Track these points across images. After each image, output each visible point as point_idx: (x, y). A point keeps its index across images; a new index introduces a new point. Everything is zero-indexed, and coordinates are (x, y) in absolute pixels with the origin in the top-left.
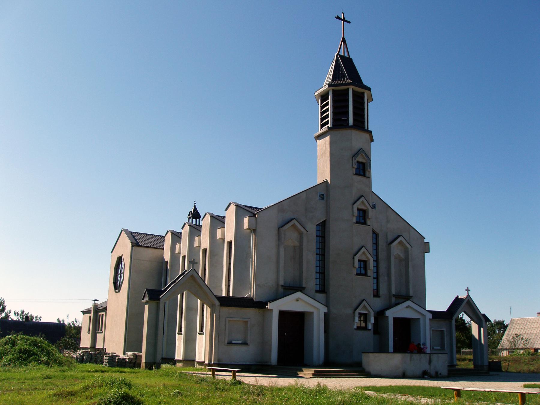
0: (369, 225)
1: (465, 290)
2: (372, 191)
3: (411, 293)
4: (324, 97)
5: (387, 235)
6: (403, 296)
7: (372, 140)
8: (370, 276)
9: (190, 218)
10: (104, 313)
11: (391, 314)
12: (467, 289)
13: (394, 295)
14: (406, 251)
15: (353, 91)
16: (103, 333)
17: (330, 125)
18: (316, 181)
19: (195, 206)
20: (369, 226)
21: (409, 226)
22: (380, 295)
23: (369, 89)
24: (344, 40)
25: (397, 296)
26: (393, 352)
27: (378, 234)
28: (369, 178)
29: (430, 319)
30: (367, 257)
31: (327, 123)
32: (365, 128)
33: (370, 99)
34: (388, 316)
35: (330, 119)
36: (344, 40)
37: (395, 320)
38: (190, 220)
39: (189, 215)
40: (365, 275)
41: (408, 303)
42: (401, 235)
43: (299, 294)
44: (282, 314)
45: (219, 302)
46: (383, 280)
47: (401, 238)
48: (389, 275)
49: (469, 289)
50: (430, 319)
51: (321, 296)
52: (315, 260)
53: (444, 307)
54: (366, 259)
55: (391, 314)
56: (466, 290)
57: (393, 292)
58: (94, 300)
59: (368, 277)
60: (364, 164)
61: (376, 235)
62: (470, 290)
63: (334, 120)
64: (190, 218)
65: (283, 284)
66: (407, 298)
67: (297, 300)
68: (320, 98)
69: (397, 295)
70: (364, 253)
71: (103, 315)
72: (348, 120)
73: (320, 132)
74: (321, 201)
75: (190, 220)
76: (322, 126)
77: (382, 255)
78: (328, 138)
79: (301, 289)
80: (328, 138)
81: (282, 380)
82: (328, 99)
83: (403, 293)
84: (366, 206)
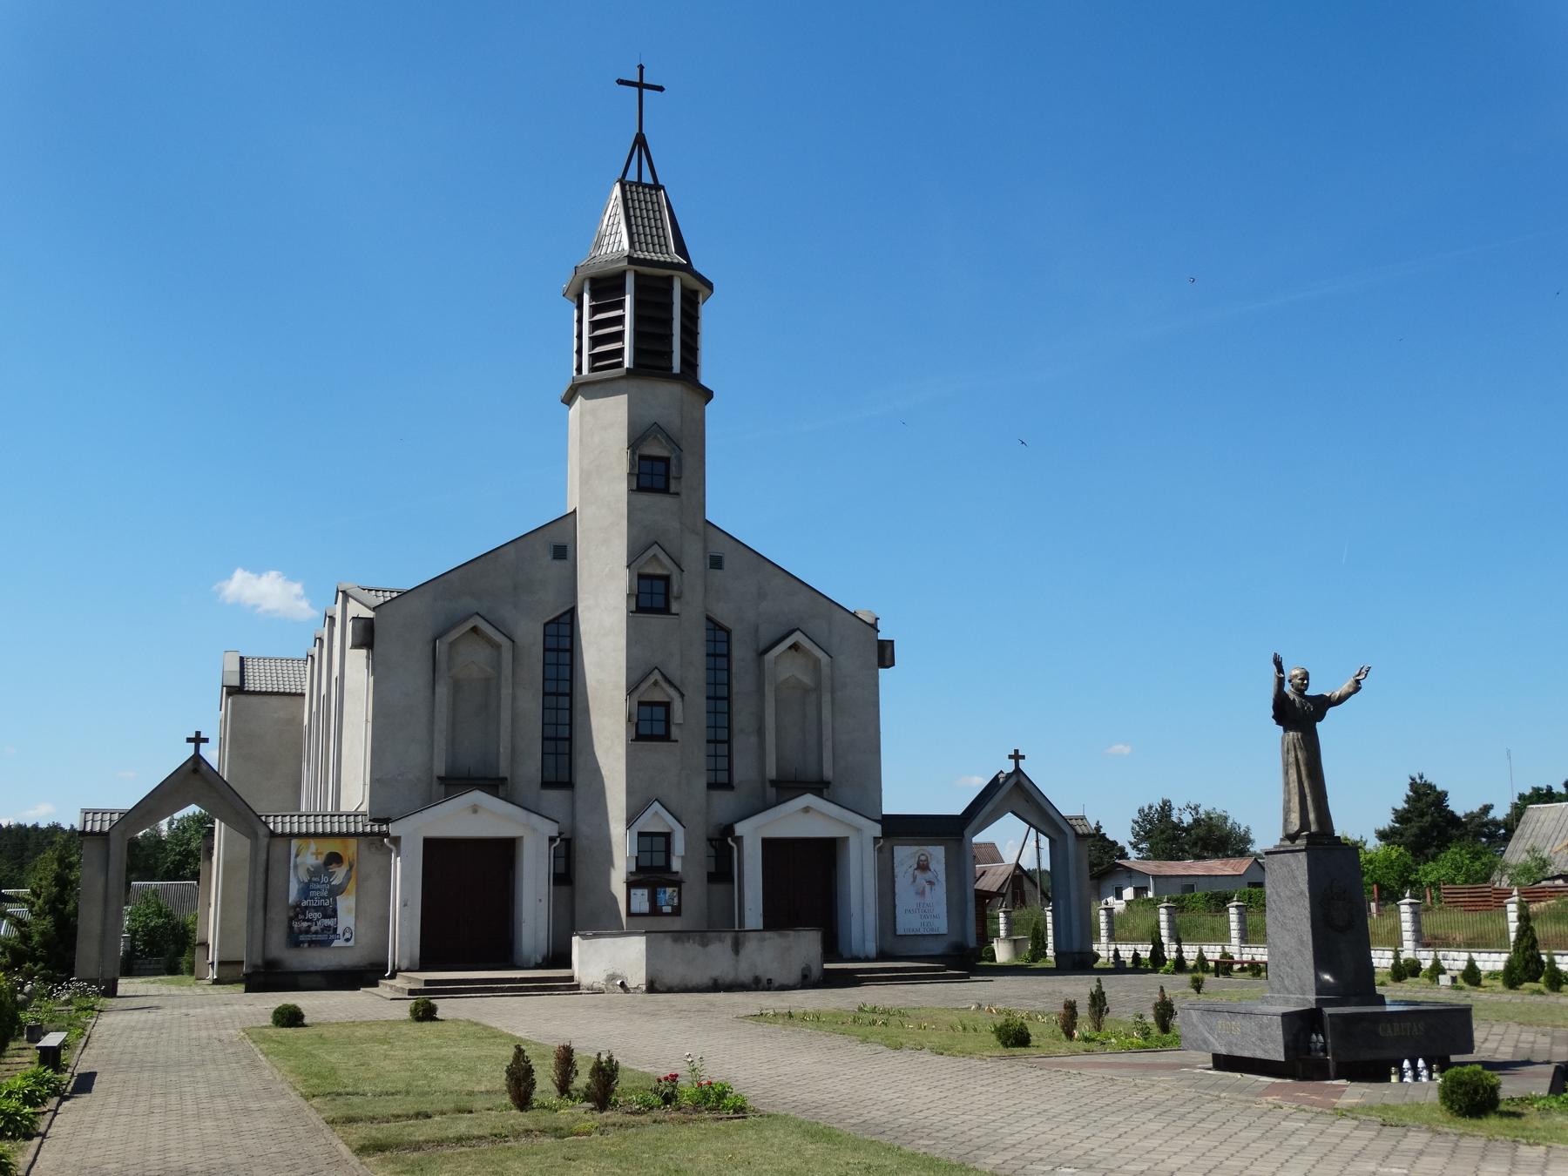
0: (677, 614)
2: (707, 521)
3: (828, 773)
5: (757, 631)
8: (677, 741)
11: (752, 833)
12: (193, 736)
13: (773, 783)
16: (1202, 980)
17: (627, 361)
18: (566, 509)
20: (676, 617)
21: (829, 602)
22: (735, 785)
23: (709, 286)
24: (640, 142)
26: (762, 928)
29: (876, 839)
30: (668, 695)
32: (672, 368)
34: (742, 837)
36: (640, 142)
42: (798, 629)
44: (771, 847)
47: (797, 637)
48: (760, 732)
50: (876, 839)
52: (705, 698)
54: (667, 700)
59: (673, 744)
63: (638, 352)
65: (443, 774)
70: (656, 683)
74: (558, 562)
77: (742, 684)
84: (665, 567)
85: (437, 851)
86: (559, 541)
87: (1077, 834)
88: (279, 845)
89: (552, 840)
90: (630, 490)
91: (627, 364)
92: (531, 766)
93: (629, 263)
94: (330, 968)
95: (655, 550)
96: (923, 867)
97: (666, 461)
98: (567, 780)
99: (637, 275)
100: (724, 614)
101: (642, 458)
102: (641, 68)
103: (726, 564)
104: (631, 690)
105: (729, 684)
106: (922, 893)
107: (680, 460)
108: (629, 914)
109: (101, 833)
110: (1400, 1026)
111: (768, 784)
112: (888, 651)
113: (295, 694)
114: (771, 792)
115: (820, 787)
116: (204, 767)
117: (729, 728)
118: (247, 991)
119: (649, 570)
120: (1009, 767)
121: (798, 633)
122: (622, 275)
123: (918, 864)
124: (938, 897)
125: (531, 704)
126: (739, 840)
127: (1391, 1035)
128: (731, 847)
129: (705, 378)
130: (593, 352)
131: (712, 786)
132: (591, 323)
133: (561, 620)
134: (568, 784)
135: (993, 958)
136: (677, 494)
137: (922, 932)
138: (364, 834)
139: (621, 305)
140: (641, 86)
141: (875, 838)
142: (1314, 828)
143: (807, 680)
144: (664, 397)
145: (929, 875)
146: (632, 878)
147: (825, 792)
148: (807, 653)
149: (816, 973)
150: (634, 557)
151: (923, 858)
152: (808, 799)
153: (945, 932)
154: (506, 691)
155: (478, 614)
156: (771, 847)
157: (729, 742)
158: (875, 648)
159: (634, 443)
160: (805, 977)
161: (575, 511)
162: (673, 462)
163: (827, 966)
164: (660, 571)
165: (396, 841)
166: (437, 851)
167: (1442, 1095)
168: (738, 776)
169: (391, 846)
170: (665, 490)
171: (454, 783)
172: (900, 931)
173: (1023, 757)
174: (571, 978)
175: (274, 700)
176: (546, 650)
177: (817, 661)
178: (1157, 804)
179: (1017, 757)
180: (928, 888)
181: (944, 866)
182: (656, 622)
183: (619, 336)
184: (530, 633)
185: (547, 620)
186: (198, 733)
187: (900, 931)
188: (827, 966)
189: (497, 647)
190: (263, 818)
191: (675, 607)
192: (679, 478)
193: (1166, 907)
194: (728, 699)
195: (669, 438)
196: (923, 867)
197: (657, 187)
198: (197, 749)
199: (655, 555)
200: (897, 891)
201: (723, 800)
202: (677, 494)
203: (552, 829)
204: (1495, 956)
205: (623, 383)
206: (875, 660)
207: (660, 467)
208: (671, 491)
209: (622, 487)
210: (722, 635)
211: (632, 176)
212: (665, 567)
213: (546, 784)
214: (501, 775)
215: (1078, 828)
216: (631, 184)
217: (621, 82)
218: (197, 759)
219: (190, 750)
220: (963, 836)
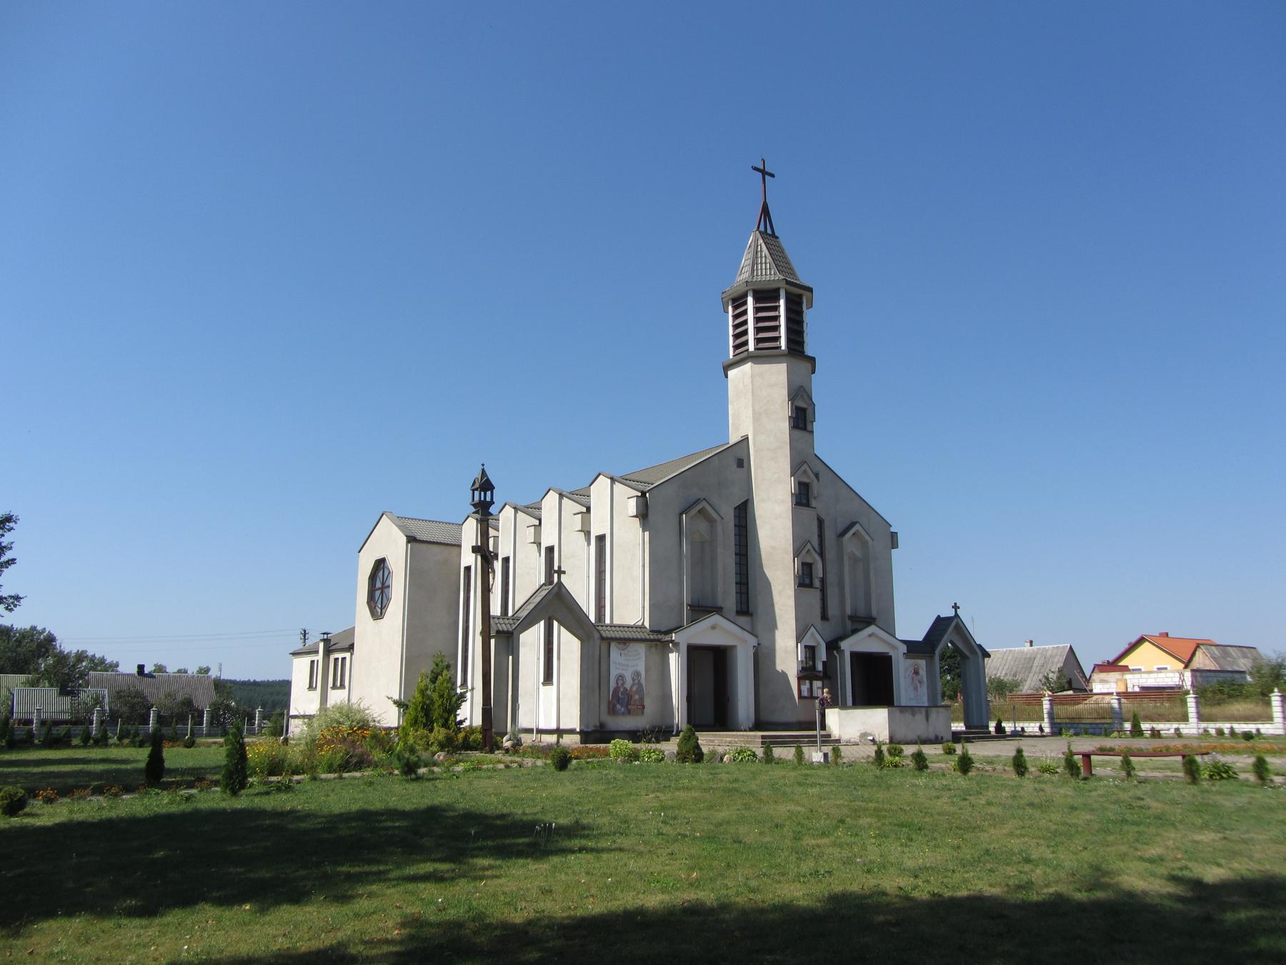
1: (961, 607)
2: (815, 455)
3: (874, 613)
6: (861, 617)
7: (813, 372)
9: (477, 489)
10: (347, 655)
12: (562, 569)
13: (850, 617)
14: (864, 544)
19: (483, 470)
23: (810, 290)
24: (765, 211)
25: (853, 618)
27: (824, 521)
28: (812, 432)
32: (781, 347)
33: (810, 306)
36: (765, 211)
37: (854, 655)
38: (477, 493)
39: (473, 484)
40: (811, 585)
41: (872, 629)
43: (716, 619)
45: (774, 636)
46: (832, 592)
47: (857, 527)
48: (841, 586)
49: (562, 569)
51: (743, 620)
53: (919, 636)
55: (851, 645)
56: (953, 607)
57: (849, 611)
58: (324, 634)
60: (804, 410)
61: (821, 522)
62: (564, 572)
64: (477, 489)
66: (869, 621)
67: (713, 627)
68: (730, 303)
69: (695, 606)
71: (344, 659)
75: (477, 493)
79: (719, 610)
83: (862, 612)
84: (808, 477)
87: (601, 636)
91: (783, 348)
92: (729, 600)
94: (632, 729)
104: (797, 553)
108: (800, 696)
112: (895, 538)
113: (455, 545)
116: (563, 590)
122: (777, 290)
128: (836, 657)
129: (809, 350)
132: (733, 326)
135: (1005, 732)
139: (776, 308)
145: (919, 677)
146: (801, 675)
158: (890, 534)
161: (746, 439)
167: (157, 697)
175: (435, 548)
182: (804, 510)
183: (776, 328)
191: (814, 503)
204: (1032, 725)
205: (785, 358)
206: (890, 547)
209: (785, 425)
212: (808, 477)
215: (602, 632)
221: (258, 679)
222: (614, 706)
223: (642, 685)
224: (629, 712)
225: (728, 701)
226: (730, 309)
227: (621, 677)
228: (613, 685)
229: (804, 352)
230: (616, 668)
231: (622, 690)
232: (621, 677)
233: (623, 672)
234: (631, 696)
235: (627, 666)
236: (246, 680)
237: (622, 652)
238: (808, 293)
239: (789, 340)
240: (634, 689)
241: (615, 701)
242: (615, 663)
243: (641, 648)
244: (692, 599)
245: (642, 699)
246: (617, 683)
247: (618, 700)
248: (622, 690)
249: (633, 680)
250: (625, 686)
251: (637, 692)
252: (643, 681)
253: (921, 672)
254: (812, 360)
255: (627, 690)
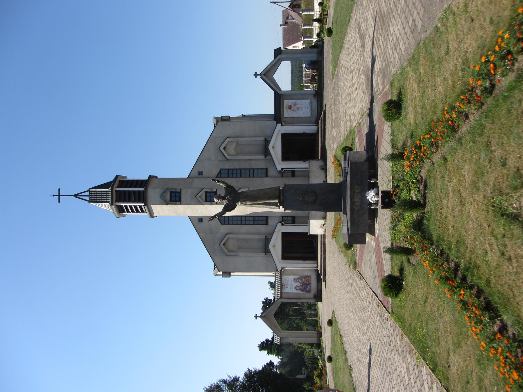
4: (121, 210)
7: (156, 177)
11: (280, 165)
12: (255, 315)
13: (265, 157)
15: (118, 187)
17: (142, 204)
23: (117, 177)
24: (76, 196)
29: (282, 125)
31: (140, 207)
32: (143, 191)
33: (125, 177)
35: (138, 205)
36: (76, 196)
44: (285, 158)
47: (222, 148)
50: (282, 125)
57: (262, 157)
63: (139, 201)
65: (264, 253)
72: (139, 192)
73: (147, 214)
74: (203, 221)
76: (143, 212)
77: (236, 166)
78: (153, 207)
80: (153, 207)
81: (326, 61)
82: (122, 206)
84: (203, 194)
85: (285, 257)
86: (197, 221)
88: (284, 295)
89: (283, 225)
90: (181, 204)
92: (262, 228)
93: (113, 205)
94: (316, 281)
95: (198, 197)
96: (290, 107)
97: (171, 193)
98: (265, 170)
99: (116, 201)
100: (215, 172)
101: (171, 201)
102: (54, 196)
103: (201, 170)
105: (237, 169)
106: (298, 108)
107: (171, 189)
109: (280, 339)
110: (356, 198)
111: (266, 158)
112: (225, 118)
114: (268, 157)
115: (267, 142)
117: (249, 169)
118: (321, 301)
119: (204, 198)
120: (259, 77)
121: (220, 148)
123: (289, 109)
124: (300, 103)
125: (244, 228)
126: (282, 169)
127: (359, 203)
129: (144, 177)
130: (140, 211)
131: (267, 176)
133: (220, 219)
134: (267, 218)
136: (181, 190)
137: (310, 108)
138: (281, 274)
140: (59, 196)
141: (282, 126)
142: (277, 201)
143: (234, 145)
144: (152, 193)
145: (293, 106)
147: (268, 140)
148: (227, 145)
149: (321, 163)
150: (199, 203)
151: (287, 107)
152: (270, 147)
153: (310, 100)
154: (241, 236)
155: (219, 245)
156: (285, 158)
157: (254, 169)
159: (167, 203)
160: (323, 169)
162: (171, 191)
163: (319, 158)
164: (204, 195)
165: (282, 268)
166: (285, 257)
168: (264, 167)
169: (284, 269)
170: (180, 193)
171: (267, 251)
172: (310, 115)
173: (256, 73)
174: (321, 235)
176: (229, 224)
177: (229, 142)
178: (269, 361)
179: (256, 75)
180: (297, 106)
181: (290, 100)
183: (135, 206)
184: (225, 228)
185: (220, 224)
186: (254, 317)
187: (310, 115)
188: (319, 158)
189: (228, 239)
190: (277, 299)
191: (215, 190)
192: (176, 189)
193: (303, 13)
194: (241, 169)
195: (164, 192)
196: (290, 107)
197: (89, 191)
198: (258, 317)
199: (199, 197)
200: (297, 116)
201: (271, 172)
202: (181, 190)
203: (279, 225)
205: (149, 206)
207: (173, 194)
208: (180, 191)
210: (222, 171)
211: (87, 198)
213: (267, 224)
214: (264, 140)
216: (90, 199)
217: (59, 202)
218: (261, 317)
219: (259, 319)
220: (281, 94)
221: (290, 69)
222: (307, 291)
223: (299, 277)
224: (310, 284)
225: (305, 133)
226: (124, 214)
227: (296, 288)
228: (299, 291)
229: (146, 180)
230: (292, 290)
231: (301, 287)
232: (296, 288)
233: (294, 286)
234: (303, 283)
235: (291, 285)
236: (291, 74)
237: (286, 287)
238: (119, 178)
239: (140, 187)
240: (300, 281)
241: (306, 290)
242: (290, 290)
243: (284, 277)
244: (263, 252)
245: (304, 277)
246: (298, 289)
247: (305, 289)
248: (301, 287)
249: (297, 282)
250: (299, 286)
251: (302, 280)
252: (297, 277)
253: (290, 104)
254: (150, 177)
255: (301, 285)
